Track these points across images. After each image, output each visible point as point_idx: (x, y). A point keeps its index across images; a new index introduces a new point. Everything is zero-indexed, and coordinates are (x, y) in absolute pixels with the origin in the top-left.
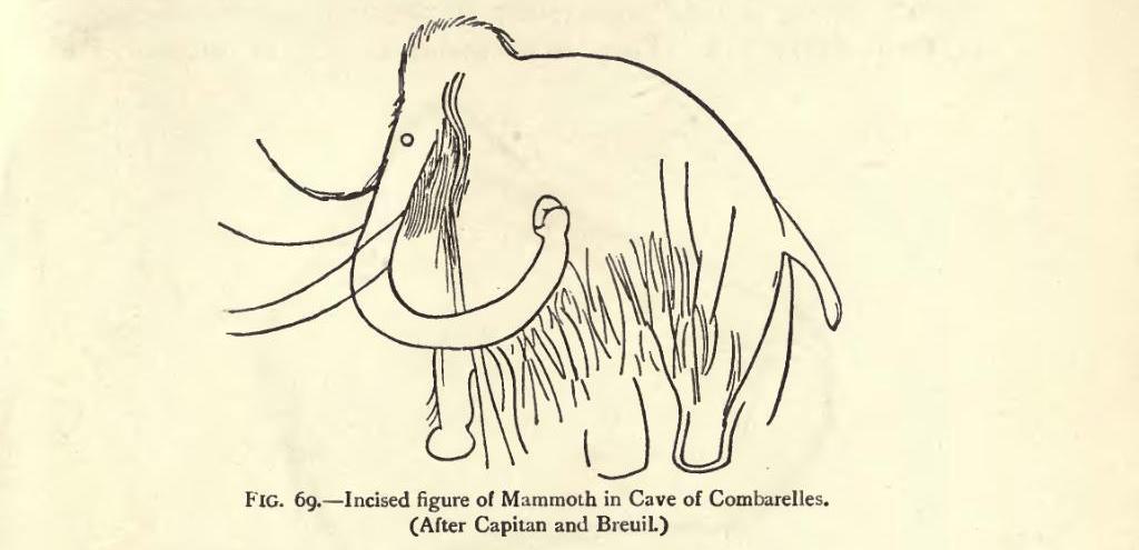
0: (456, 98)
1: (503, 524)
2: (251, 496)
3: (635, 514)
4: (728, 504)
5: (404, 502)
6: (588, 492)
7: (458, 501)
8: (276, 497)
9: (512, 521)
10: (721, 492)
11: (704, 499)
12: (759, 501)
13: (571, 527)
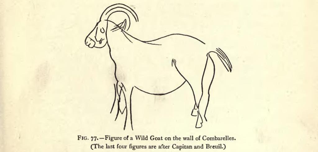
0: (131, 12)
1: (180, 146)
2: (79, 137)
3: (199, 143)
6: (176, 136)
7: (222, 139)
8: (86, 137)
9: (182, 146)
10: (175, 145)
11: (201, 138)
12: (216, 139)
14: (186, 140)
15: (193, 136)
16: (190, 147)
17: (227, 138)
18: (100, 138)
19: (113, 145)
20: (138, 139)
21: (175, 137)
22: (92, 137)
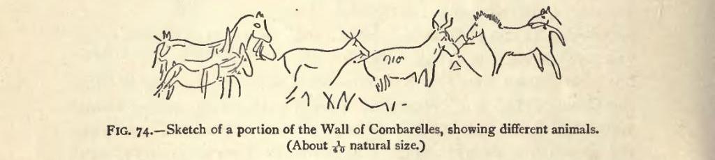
2: (111, 128)
4: (381, 133)
5: (241, 130)
6: (305, 125)
7: (529, 130)
8: (126, 128)
10: (377, 125)
11: (366, 129)
13: (407, 147)
14: (330, 131)
15: (347, 125)
16: (571, 130)
17: (427, 129)
18: (295, 80)
19: (188, 127)
20: (328, 131)
21: (303, 127)
22: (138, 129)
